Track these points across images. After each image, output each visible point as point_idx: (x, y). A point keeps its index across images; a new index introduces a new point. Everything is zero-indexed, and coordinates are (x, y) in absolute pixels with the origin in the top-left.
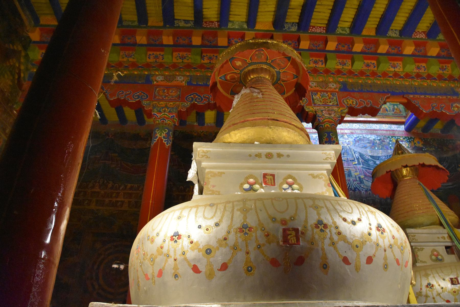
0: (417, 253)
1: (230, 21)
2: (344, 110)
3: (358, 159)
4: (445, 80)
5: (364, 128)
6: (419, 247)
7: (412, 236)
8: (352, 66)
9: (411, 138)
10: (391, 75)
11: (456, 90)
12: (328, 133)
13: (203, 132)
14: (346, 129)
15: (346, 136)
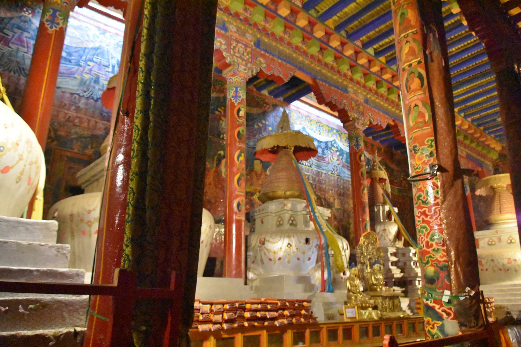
1: (315, 9)
3: (113, 67)
4: (230, 14)
8: (231, 3)
10: (302, 51)
11: (227, 25)
12: (55, 11)
15: (108, 35)
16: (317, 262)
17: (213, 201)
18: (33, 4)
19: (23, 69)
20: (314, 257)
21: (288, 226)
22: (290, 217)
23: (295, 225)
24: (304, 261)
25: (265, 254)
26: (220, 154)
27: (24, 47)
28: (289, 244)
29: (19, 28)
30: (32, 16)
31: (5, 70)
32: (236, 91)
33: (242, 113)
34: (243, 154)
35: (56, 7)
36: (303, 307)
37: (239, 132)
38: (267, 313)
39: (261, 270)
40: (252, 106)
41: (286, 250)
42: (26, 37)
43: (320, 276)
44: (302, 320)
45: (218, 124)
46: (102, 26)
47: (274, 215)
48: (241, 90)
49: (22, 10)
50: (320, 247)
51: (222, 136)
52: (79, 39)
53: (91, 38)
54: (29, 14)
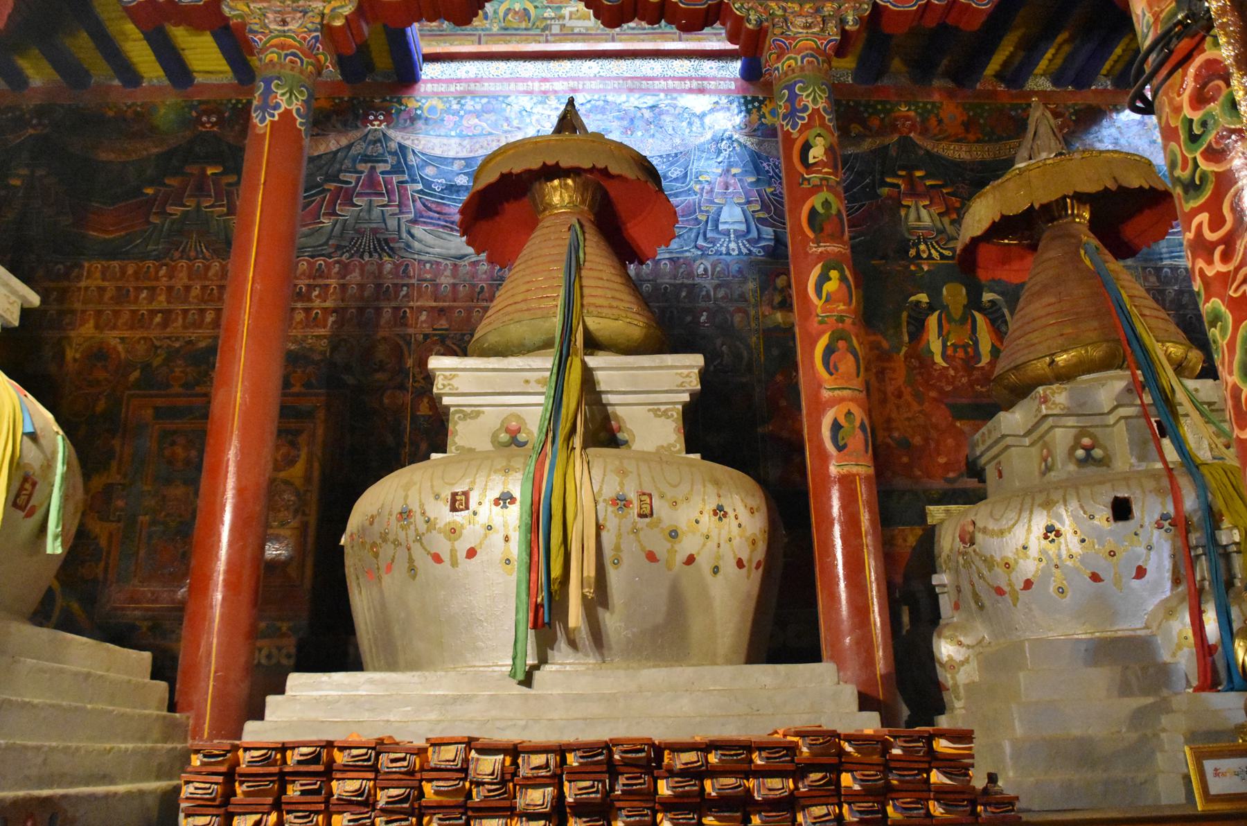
0: (456, 423)
2: (342, 7)
5: (614, 74)
6: (468, 410)
7: (446, 377)
9: (752, 101)
13: (133, 104)
14: (559, 79)
16: (1176, 581)
17: (917, 440)
18: (384, 100)
19: (386, 241)
20: (1161, 562)
21: (1072, 467)
22: (1077, 439)
23: (1104, 462)
24: (1118, 581)
25: (981, 577)
26: (918, 303)
27: (382, 195)
28: (1050, 529)
29: (366, 159)
30: (387, 126)
31: (352, 256)
32: (793, 97)
33: (817, 153)
34: (834, 274)
35: (269, 73)
36: (935, 759)
37: (813, 211)
38: (752, 783)
39: (982, 631)
40: (1000, 139)
41: (1043, 552)
42: (382, 173)
43: (1189, 632)
44: (936, 809)
45: (896, 220)
46: (536, 86)
47: (1027, 441)
48: (803, 89)
49: (366, 121)
50: (1179, 524)
51: (912, 252)
52: (490, 134)
53: (515, 123)
54: (381, 122)
